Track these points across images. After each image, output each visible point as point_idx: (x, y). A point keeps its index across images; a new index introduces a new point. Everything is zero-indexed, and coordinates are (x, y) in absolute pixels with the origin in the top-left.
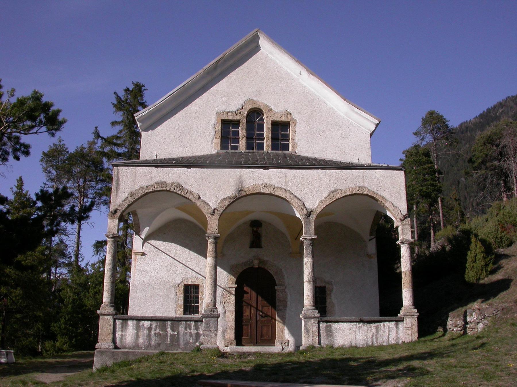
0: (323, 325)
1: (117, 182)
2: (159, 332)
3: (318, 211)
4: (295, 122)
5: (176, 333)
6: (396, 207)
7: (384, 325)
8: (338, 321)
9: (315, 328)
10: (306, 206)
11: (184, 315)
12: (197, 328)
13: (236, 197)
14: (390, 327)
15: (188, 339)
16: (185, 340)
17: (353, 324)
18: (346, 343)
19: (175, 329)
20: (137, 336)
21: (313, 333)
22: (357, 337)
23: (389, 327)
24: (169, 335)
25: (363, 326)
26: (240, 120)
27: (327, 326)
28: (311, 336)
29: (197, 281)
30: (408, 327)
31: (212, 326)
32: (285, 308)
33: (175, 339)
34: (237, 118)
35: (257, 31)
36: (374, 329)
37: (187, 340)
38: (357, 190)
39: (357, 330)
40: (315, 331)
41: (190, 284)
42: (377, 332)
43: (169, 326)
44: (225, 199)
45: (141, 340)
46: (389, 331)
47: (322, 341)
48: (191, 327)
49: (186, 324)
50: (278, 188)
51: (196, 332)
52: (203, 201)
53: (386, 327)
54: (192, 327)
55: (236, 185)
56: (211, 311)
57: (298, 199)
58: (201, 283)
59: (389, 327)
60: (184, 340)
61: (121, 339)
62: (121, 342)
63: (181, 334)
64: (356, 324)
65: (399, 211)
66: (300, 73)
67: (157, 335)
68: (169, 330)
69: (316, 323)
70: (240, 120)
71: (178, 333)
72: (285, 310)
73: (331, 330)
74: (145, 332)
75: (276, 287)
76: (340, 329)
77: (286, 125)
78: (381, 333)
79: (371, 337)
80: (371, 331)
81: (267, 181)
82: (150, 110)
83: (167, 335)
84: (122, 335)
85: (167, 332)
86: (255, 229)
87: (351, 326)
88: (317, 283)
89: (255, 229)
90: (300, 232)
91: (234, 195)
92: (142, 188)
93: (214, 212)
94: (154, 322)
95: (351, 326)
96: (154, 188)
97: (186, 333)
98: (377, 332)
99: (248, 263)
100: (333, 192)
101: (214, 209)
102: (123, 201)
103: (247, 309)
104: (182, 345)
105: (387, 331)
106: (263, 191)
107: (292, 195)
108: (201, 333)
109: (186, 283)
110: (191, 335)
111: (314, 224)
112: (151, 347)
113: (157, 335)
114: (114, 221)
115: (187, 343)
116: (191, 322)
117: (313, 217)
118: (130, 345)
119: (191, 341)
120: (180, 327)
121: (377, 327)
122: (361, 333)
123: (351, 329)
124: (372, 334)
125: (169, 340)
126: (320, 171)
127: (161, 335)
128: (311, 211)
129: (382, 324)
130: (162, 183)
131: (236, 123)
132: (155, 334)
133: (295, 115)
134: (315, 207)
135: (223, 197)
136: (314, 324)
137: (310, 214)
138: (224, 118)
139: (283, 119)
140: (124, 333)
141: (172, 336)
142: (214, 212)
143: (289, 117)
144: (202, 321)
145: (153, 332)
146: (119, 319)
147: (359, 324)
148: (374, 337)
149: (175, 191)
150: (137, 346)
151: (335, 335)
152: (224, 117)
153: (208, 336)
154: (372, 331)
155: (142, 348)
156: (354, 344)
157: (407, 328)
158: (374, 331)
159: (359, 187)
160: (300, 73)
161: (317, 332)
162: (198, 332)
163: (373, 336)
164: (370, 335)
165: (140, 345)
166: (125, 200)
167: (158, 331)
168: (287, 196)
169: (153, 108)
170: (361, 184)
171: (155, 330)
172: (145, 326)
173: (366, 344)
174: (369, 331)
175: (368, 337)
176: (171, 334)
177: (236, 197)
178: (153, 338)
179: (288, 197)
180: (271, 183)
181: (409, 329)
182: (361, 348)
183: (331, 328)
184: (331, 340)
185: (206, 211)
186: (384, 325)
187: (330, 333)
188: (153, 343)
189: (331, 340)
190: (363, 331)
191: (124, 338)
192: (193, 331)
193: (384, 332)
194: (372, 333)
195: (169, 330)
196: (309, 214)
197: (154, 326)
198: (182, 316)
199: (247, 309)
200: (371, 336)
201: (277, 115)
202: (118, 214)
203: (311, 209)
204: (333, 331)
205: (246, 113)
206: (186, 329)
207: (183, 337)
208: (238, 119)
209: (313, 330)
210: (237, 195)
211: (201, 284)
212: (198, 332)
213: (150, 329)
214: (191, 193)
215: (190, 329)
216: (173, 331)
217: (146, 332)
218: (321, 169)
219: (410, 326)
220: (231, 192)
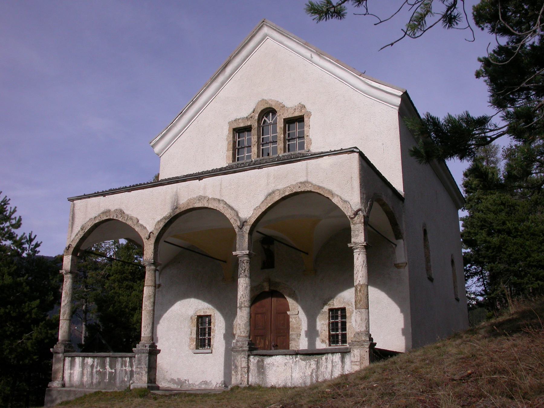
0: (254, 360)
1: (72, 217)
2: (99, 370)
3: (253, 220)
5: (113, 371)
6: (345, 202)
7: (326, 359)
8: (322, 352)
10: (240, 215)
12: (131, 366)
14: (334, 361)
15: (123, 377)
17: (288, 357)
19: (113, 366)
20: (82, 374)
22: (293, 375)
23: (332, 362)
24: (108, 373)
25: (300, 360)
26: (251, 125)
27: (258, 361)
28: (239, 373)
31: (142, 363)
32: (298, 338)
33: (113, 377)
34: (249, 123)
35: (263, 21)
36: (314, 365)
37: (122, 378)
38: (297, 188)
39: (293, 365)
40: (244, 367)
41: (202, 315)
42: (318, 368)
44: (161, 220)
45: (85, 379)
46: (333, 366)
47: (250, 379)
49: (122, 361)
51: (131, 369)
52: (142, 225)
53: (330, 361)
54: (127, 364)
55: (172, 202)
56: (143, 346)
57: (233, 209)
59: (332, 362)
60: (120, 379)
62: (70, 380)
63: (118, 372)
65: (349, 206)
66: (311, 56)
67: (98, 372)
68: (108, 367)
69: (245, 358)
70: (251, 125)
71: (115, 370)
72: (299, 339)
74: (89, 370)
75: (288, 313)
76: (273, 365)
78: (322, 369)
79: (311, 375)
81: (201, 193)
82: (163, 133)
83: (105, 373)
84: (71, 373)
85: (106, 369)
86: (266, 247)
87: (287, 361)
92: (91, 219)
93: (149, 237)
94: (96, 360)
95: (287, 361)
96: (100, 219)
97: (122, 370)
98: (318, 368)
102: (75, 236)
103: (262, 340)
104: (118, 384)
105: (330, 366)
109: (199, 314)
111: (247, 237)
112: (93, 385)
113: (98, 372)
115: (123, 381)
116: (126, 358)
117: (247, 228)
118: (77, 383)
119: (126, 379)
121: (318, 363)
122: (297, 369)
123: (286, 365)
124: (311, 371)
125: (107, 378)
128: (245, 222)
129: (324, 358)
130: (107, 212)
131: (248, 129)
132: (97, 371)
133: (309, 108)
137: (243, 225)
138: (235, 127)
139: (297, 114)
141: (111, 373)
142: (149, 237)
145: (95, 370)
146: (69, 357)
147: (296, 358)
148: (314, 375)
149: (117, 219)
150: (82, 384)
152: (236, 126)
153: (139, 374)
154: (311, 366)
156: (289, 385)
157: (355, 362)
158: (314, 366)
159: (301, 183)
160: (311, 56)
161: (246, 368)
162: (132, 370)
163: (312, 373)
164: (309, 372)
165: (84, 383)
166: (77, 235)
167: (99, 368)
168: (220, 207)
169: (165, 131)
170: (303, 180)
171: (97, 368)
172: (89, 364)
173: (304, 383)
174: (307, 368)
175: (306, 374)
176: (109, 372)
178: (95, 376)
181: (357, 363)
182: (290, 388)
184: (263, 378)
185: (144, 236)
186: (326, 358)
187: (261, 369)
188: (95, 381)
189: (263, 378)
190: (300, 367)
191: (72, 376)
192: (128, 369)
193: (326, 368)
194: (311, 370)
195: (108, 367)
196: (243, 223)
197: (95, 363)
198: (328, 347)
199: (262, 340)
200: (309, 373)
201: (289, 111)
203: (246, 219)
205: (257, 115)
206: (122, 367)
207: (120, 375)
209: (243, 366)
211: (212, 315)
212: (132, 370)
215: (126, 366)
217: (89, 369)
218: (258, 169)
219: (359, 360)
220: (165, 212)
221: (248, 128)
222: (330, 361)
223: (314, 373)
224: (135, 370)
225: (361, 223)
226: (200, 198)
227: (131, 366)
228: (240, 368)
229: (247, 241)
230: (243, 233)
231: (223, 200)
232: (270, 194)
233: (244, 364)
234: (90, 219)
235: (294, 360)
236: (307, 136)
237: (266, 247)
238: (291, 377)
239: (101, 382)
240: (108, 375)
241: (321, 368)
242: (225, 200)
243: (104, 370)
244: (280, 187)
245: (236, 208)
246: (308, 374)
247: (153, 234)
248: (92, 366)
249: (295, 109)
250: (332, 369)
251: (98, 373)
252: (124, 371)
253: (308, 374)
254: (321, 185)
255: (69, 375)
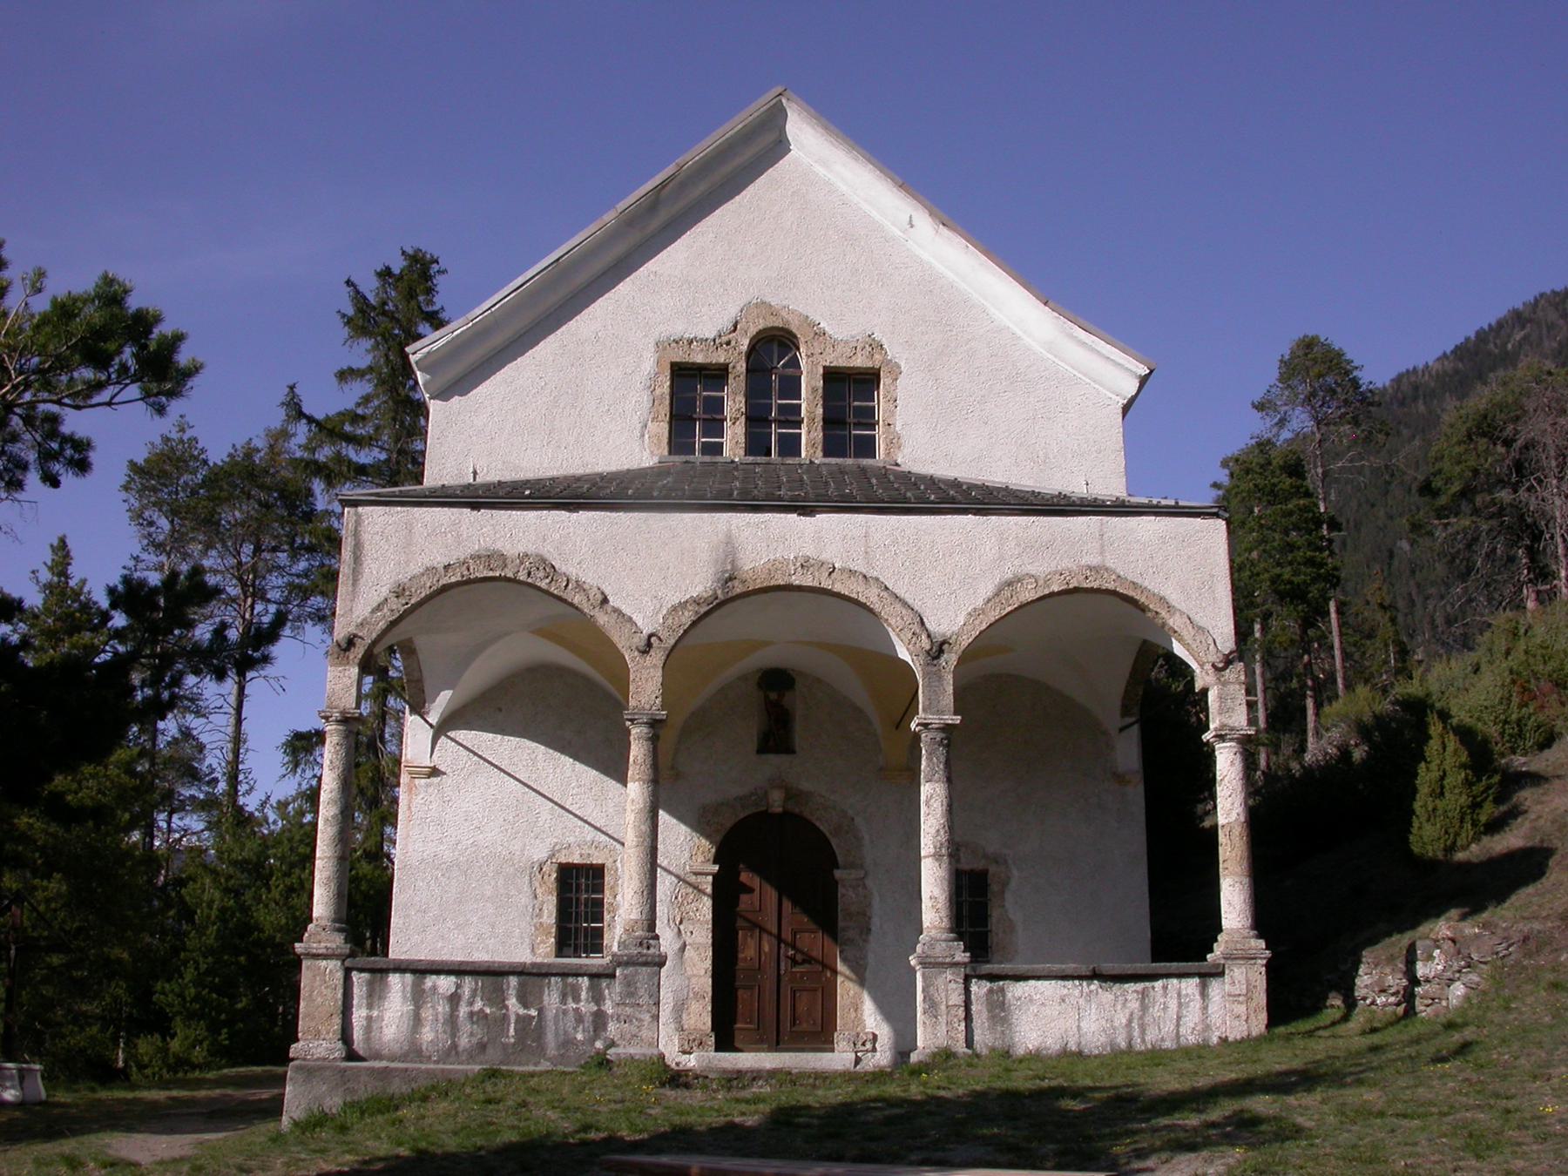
0: (979, 989)
1: (354, 553)
3: (965, 641)
5: (534, 1013)
6: (1200, 629)
7: (1165, 988)
14: (1184, 992)
17: (1069, 984)
19: (531, 999)
20: (417, 1020)
22: (1082, 1025)
25: (1100, 990)
26: (728, 365)
27: (991, 991)
31: (641, 992)
32: (864, 937)
33: (531, 1032)
34: (720, 357)
37: (566, 1033)
39: (1082, 1001)
41: (575, 862)
42: (1144, 1008)
44: (683, 605)
45: (427, 1035)
46: (1180, 1005)
47: (978, 1037)
49: (565, 985)
51: (596, 1008)
52: (616, 610)
53: (1172, 993)
54: (584, 995)
56: (641, 944)
57: (905, 604)
59: (1179, 995)
60: (557, 1034)
63: (550, 1014)
66: (911, 220)
67: (476, 1017)
68: (512, 1002)
69: (956, 982)
70: (728, 365)
71: (541, 1011)
72: (866, 941)
74: (440, 1009)
75: (838, 874)
76: (1031, 1000)
78: (1155, 1011)
81: (810, 551)
82: (456, 333)
83: (505, 1018)
84: (369, 1019)
85: (506, 1007)
87: (1066, 991)
92: (430, 570)
93: (649, 645)
95: (1066, 991)
96: (466, 573)
97: (565, 1012)
98: (1144, 1008)
103: (749, 939)
104: (552, 1050)
105: (1173, 1004)
111: (951, 682)
112: (457, 1053)
113: (476, 1017)
117: (950, 659)
118: (396, 1048)
119: (580, 1037)
121: (1144, 994)
122: (1094, 1011)
123: (1063, 1001)
124: (1127, 1015)
125: (512, 1032)
128: (944, 643)
129: (1159, 984)
131: (716, 375)
132: (471, 1014)
133: (893, 351)
137: (941, 651)
138: (678, 360)
139: (860, 361)
141: (523, 1021)
142: (649, 645)
145: (463, 1010)
147: (1088, 985)
148: (1135, 1025)
149: (530, 580)
150: (414, 1051)
152: (680, 356)
157: (1235, 996)
158: (1134, 1005)
159: (1090, 568)
160: (911, 220)
161: (962, 1009)
162: (599, 1010)
163: (1130, 1021)
164: (1121, 1019)
165: (424, 1048)
167: (478, 1005)
168: (870, 596)
170: (1094, 560)
171: (471, 1004)
173: (1111, 1045)
175: (1116, 1024)
176: (518, 1015)
181: (1241, 999)
184: (1003, 1032)
185: (625, 643)
187: (999, 1010)
188: (464, 1041)
189: (1003, 1032)
190: (1100, 1004)
193: (1165, 1008)
195: (512, 1002)
196: (938, 649)
198: (552, 960)
200: (1124, 1021)
201: (839, 349)
203: (944, 635)
205: (746, 342)
206: (563, 1001)
207: (556, 1024)
209: (950, 1003)
212: (599, 1010)
215: (577, 999)
217: (443, 1008)
219: (1244, 992)
220: (699, 583)
221: (709, 370)
222: (1172, 993)
223: (1136, 1021)
224: (610, 1012)
225: (1240, 684)
226: (805, 565)
227: (598, 998)
228: (943, 1007)
229: (951, 691)
230: (940, 670)
231: (877, 579)
232: (1009, 584)
233: (957, 998)
234: (427, 569)
235: (1086, 990)
236: (889, 425)
237: (773, 696)
238: (1079, 1030)
239: (487, 1043)
240: (513, 1025)
241: (1151, 1009)
242: (881, 579)
243: (501, 1009)
244: (1039, 568)
245: (917, 606)
246: (1121, 1023)
247: (660, 640)
248: (454, 999)
249: (856, 348)
250: (1178, 1012)
251: (475, 1019)
252: (571, 1014)
253: (1121, 1023)
254: (1139, 581)
255: (365, 1023)
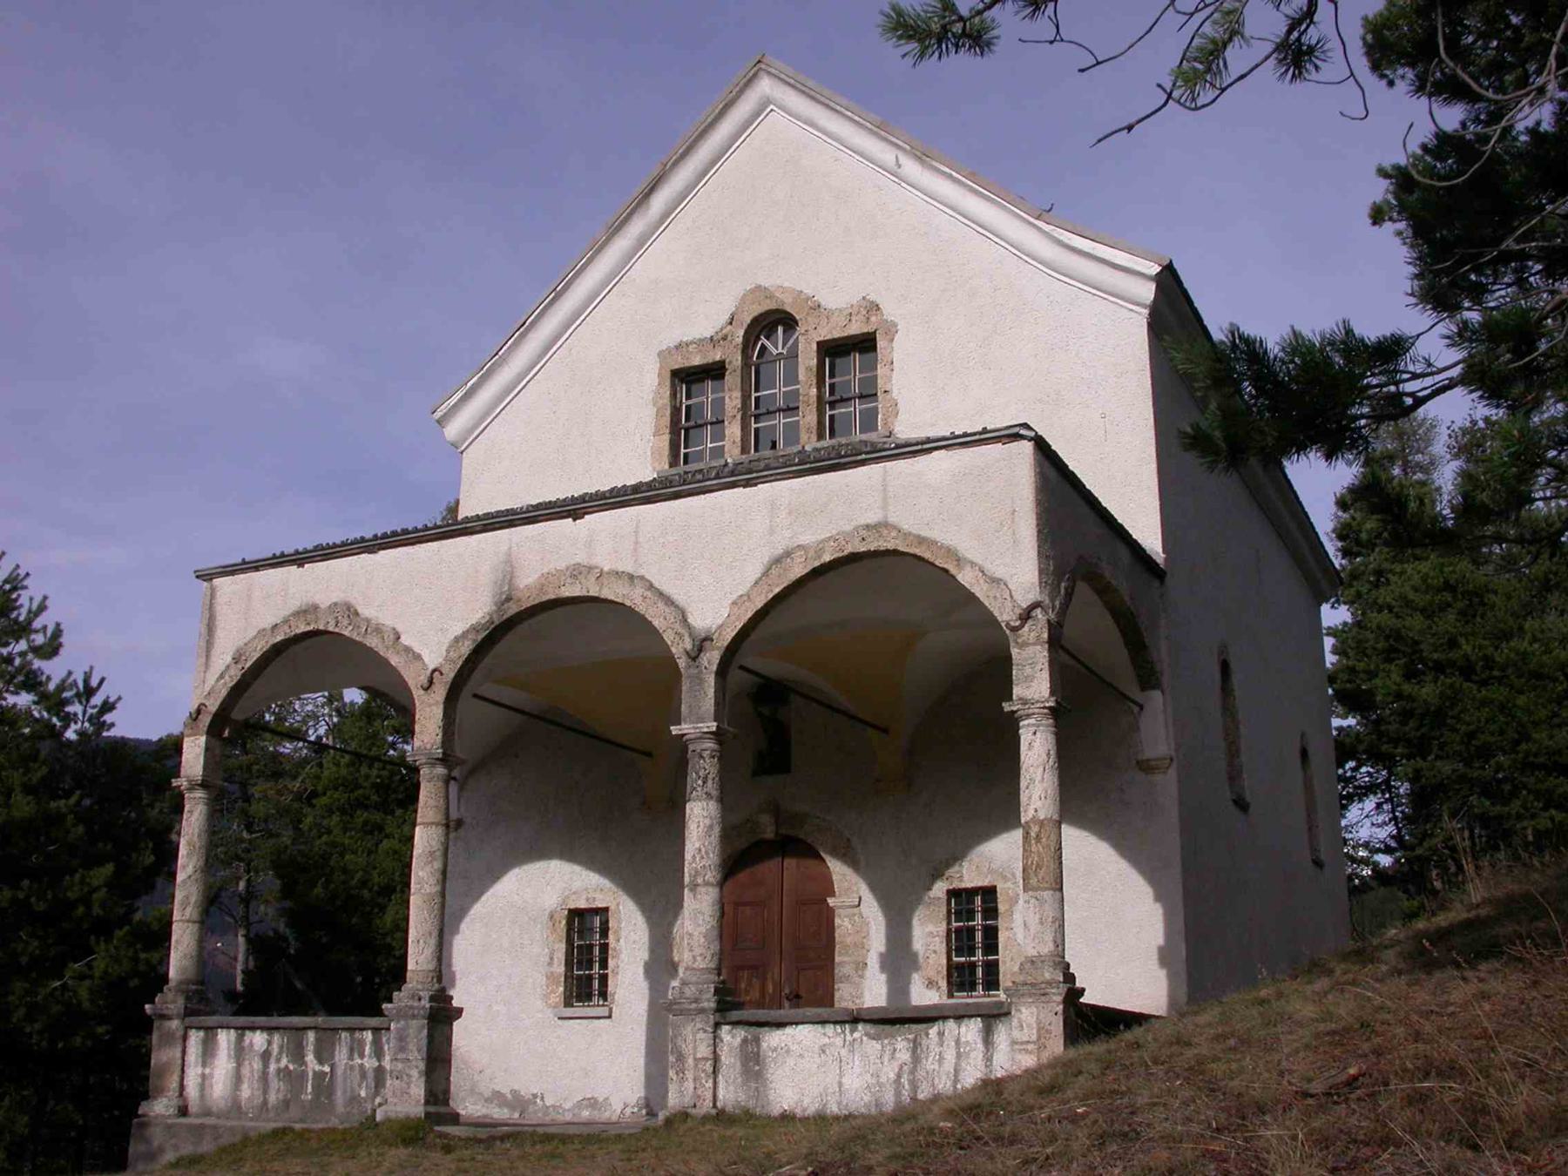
0: (731, 1038)
3: (729, 635)
4: (891, 330)
5: (327, 1069)
6: (995, 581)
7: (941, 1034)
9: (704, 1050)
11: (949, 997)
13: (493, 623)
14: (963, 1039)
16: (349, 1089)
17: (830, 1029)
18: (806, 1102)
20: (238, 1078)
21: (696, 1065)
22: (844, 1080)
23: (958, 1042)
24: (311, 1074)
25: (865, 1038)
27: (745, 1041)
28: (690, 1075)
29: (601, 897)
30: (1025, 1039)
31: (411, 1046)
32: (860, 973)
35: (759, 62)
38: (857, 540)
39: (844, 1052)
42: (916, 1060)
43: (311, 1047)
44: (464, 635)
45: (246, 1092)
46: (959, 1056)
47: (721, 1093)
48: (364, 1050)
50: (608, 573)
51: (377, 1064)
52: (408, 650)
54: (367, 1049)
58: (615, 903)
59: (958, 1042)
60: (345, 1092)
61: (202, 1087)
63: (339, 1071)
64: (843, 1032)
67: (284, 1073)
68: (310, 1058)
69: (705, 1031)
71: (332, 1067)
72: (862, 977)
73: (758, 1054)
74: (255, 1066)
76: (788, 1051)
77: (865, 344)
78: (930, 1064)
79: (895, 1081)
80: (893, 1057)
81: (581, 558)
83: (303, 1075)
84: (203, 1076)
87: (827, 1040)
88: (966, 878)
89: (766, 711)
90: (551, 722)
91: (488, 618)
92: (262, 632)
93: (431, 682)
94: (276, 1038)
97: (352, 1068)
98: (916, 1060)
99: (749, 825)
100: (777, 561)
101: (434, 671)
105: (950, 1056)
106: (567, 592)
107: (648, 594)
108: (388, 1067)
110: (363, 1075)
113: (284, 1073)
114: (197, 742)
115: (354, 1099)
116: (364, 1033)
119: (363, 1094)
120: (338, 1048)
121: (915, 1046)
122: (857, 1063)
123: (824, 1052)
125: (310, 1089)
126: (738, 491)
127: (293, 1075)
128: (705, 640)
129: (933, 1031)
130: (310, 610)
131: (715, 371)
132: (279, 1071)
133: (890, 311)
134: (720, 622)
135: (458, 629)
136: (701, 1035)
138: (677, 367)
139: (856, 328)
140: (207, 1071)
141: (319, 1076)
142: (431, 682)
143: (873, 319)
144: (388, 1029)
145: (273, 1067)
146: (199, 1028)
147: (852, 1032)
148: (904, 1080)
150: (236, 1107)
151: (771, 1071)
152: (679, 362)
155: (247, 1114)
157: (1022, 1043)
158: (904, 1056)
159: (867, 527)
162: (380, 1066)
163: (899, 1076)
165: (243, 1103)
166: (222, 676)
167: (284, 1062)
168: (634, 597)
170: (872, 517)
171: (278, 1060)
172: (256, 1048)
175: (883, 1079)
176: (315, 1072)
177: (493, 623)
178: (274, 1083)
179: (639, 600)
180: (593, 562)
181: (1030, 1047)
182: (837, 1118)
183: (759, 1046)
185: (413, 678)
187: (753, 1063)
188: (273, 1098)
190: (865, 1056)
191: (207, 1082)
192: (370, 1063)
193: (941, 1060)
194: (896, 1065)
195: (310, 1058)
196: (702, 643)
197: (275, 1048)
198: (945, 1000)
200: (892, 1076)
201: (834, 319)
202: (206, 720)
204: (764, 1059)
205: (741, 333)
206: (351, 1058)
208: (718, 358)
209: (699, 1056)
210: (494, 616)
211: (613, 907)
212: (380, 1066)
213: (266, 1056)
214: (378, 630)
215: (362, 1056)
216: (321, 1062)
217: (257, 1065)
219: (1034, 1038)
220: (476, 610)
